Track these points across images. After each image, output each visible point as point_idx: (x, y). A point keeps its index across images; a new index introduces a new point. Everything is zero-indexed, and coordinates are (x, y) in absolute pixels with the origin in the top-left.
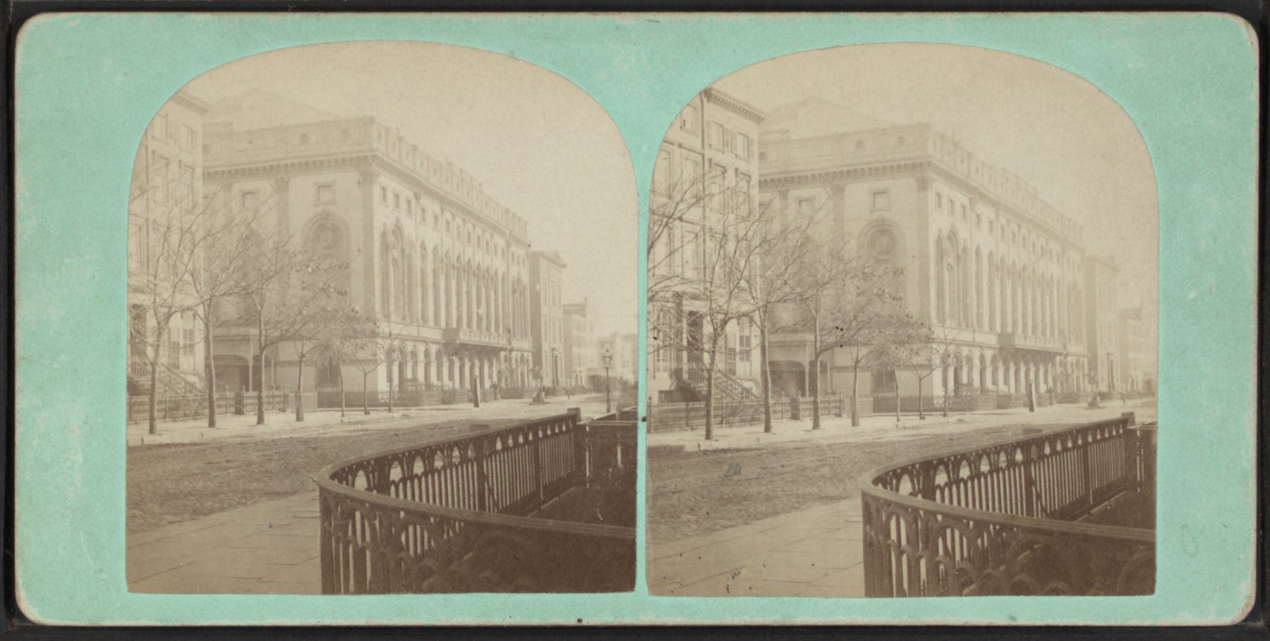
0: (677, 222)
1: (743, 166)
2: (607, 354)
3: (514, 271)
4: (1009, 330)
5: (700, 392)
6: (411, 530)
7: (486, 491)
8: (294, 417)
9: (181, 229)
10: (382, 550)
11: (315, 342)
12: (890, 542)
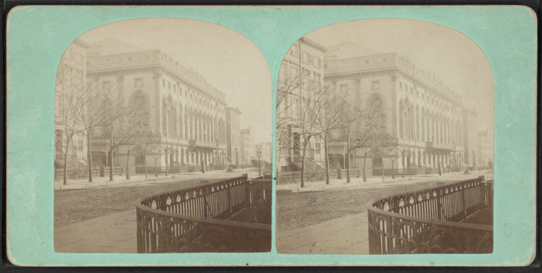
0: (289, 95)
1: (317, 71)
2: (259, 151)
3: (219, 115)
4: (431, 140)
5: (299, 167)
6: (175, 226)
7: (208, 209)
8: (125, 177)
9: (77, 97)
10: (163, 234)
11: (134, 146)
12: (380, 231)
